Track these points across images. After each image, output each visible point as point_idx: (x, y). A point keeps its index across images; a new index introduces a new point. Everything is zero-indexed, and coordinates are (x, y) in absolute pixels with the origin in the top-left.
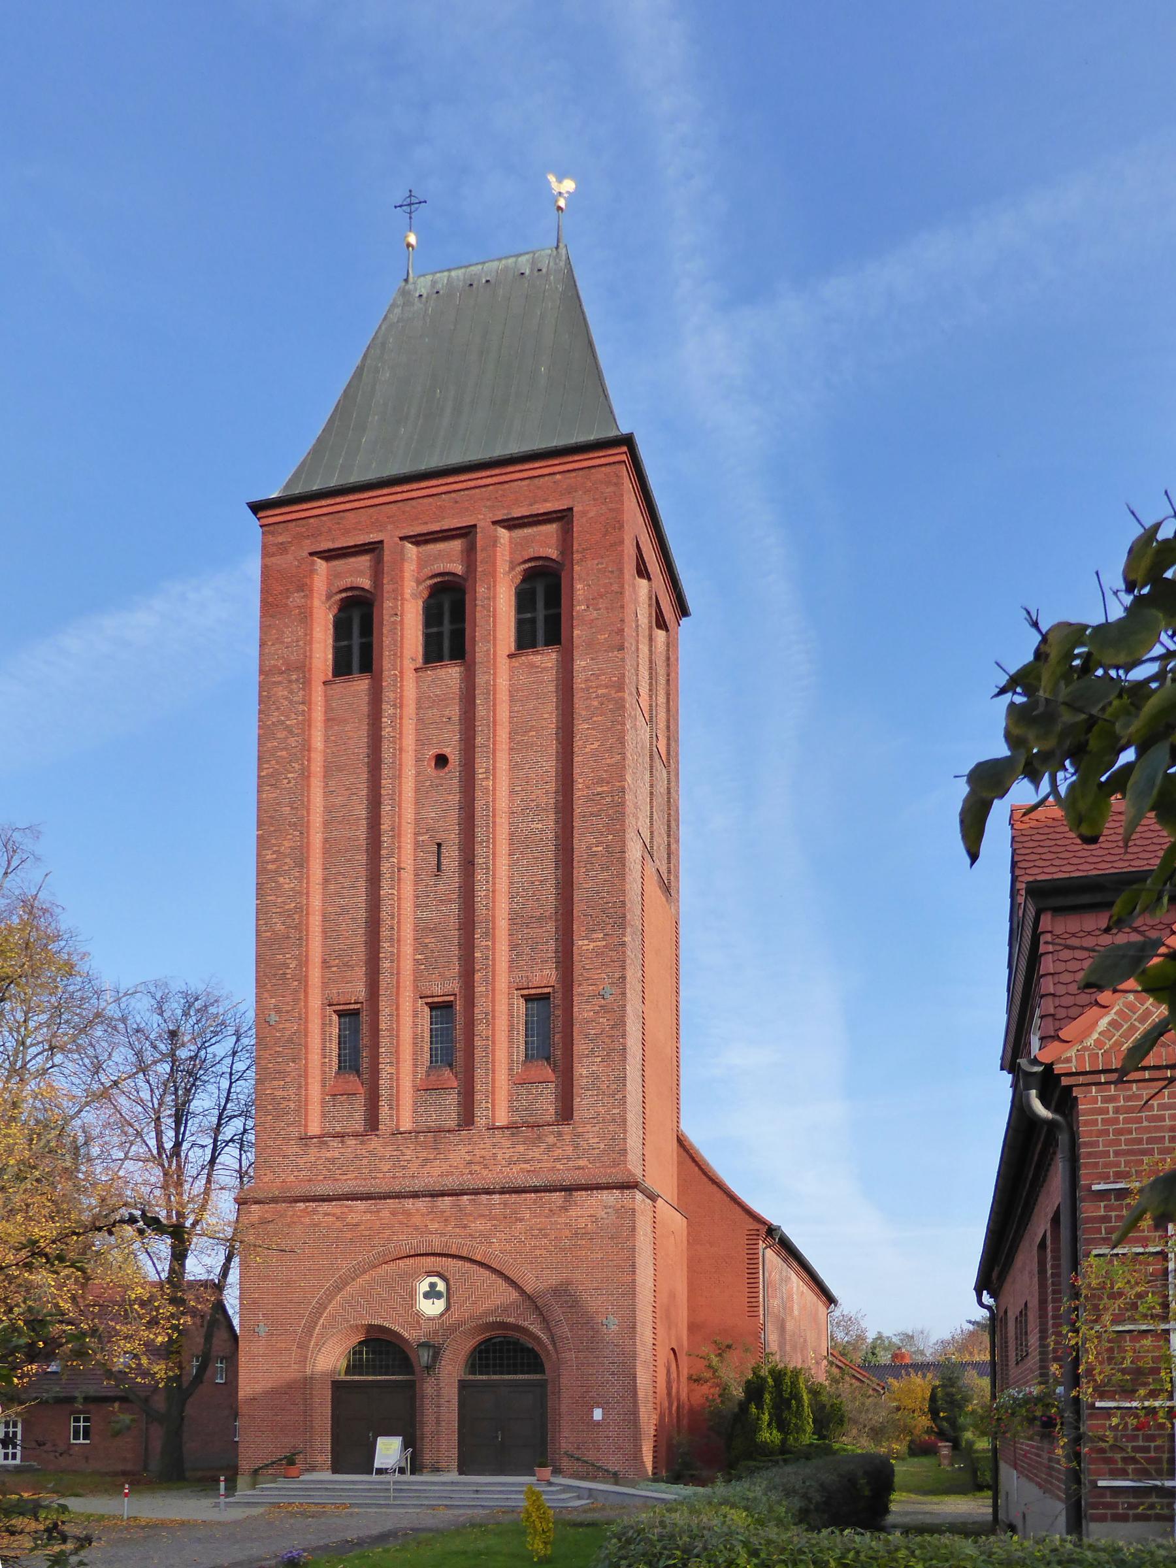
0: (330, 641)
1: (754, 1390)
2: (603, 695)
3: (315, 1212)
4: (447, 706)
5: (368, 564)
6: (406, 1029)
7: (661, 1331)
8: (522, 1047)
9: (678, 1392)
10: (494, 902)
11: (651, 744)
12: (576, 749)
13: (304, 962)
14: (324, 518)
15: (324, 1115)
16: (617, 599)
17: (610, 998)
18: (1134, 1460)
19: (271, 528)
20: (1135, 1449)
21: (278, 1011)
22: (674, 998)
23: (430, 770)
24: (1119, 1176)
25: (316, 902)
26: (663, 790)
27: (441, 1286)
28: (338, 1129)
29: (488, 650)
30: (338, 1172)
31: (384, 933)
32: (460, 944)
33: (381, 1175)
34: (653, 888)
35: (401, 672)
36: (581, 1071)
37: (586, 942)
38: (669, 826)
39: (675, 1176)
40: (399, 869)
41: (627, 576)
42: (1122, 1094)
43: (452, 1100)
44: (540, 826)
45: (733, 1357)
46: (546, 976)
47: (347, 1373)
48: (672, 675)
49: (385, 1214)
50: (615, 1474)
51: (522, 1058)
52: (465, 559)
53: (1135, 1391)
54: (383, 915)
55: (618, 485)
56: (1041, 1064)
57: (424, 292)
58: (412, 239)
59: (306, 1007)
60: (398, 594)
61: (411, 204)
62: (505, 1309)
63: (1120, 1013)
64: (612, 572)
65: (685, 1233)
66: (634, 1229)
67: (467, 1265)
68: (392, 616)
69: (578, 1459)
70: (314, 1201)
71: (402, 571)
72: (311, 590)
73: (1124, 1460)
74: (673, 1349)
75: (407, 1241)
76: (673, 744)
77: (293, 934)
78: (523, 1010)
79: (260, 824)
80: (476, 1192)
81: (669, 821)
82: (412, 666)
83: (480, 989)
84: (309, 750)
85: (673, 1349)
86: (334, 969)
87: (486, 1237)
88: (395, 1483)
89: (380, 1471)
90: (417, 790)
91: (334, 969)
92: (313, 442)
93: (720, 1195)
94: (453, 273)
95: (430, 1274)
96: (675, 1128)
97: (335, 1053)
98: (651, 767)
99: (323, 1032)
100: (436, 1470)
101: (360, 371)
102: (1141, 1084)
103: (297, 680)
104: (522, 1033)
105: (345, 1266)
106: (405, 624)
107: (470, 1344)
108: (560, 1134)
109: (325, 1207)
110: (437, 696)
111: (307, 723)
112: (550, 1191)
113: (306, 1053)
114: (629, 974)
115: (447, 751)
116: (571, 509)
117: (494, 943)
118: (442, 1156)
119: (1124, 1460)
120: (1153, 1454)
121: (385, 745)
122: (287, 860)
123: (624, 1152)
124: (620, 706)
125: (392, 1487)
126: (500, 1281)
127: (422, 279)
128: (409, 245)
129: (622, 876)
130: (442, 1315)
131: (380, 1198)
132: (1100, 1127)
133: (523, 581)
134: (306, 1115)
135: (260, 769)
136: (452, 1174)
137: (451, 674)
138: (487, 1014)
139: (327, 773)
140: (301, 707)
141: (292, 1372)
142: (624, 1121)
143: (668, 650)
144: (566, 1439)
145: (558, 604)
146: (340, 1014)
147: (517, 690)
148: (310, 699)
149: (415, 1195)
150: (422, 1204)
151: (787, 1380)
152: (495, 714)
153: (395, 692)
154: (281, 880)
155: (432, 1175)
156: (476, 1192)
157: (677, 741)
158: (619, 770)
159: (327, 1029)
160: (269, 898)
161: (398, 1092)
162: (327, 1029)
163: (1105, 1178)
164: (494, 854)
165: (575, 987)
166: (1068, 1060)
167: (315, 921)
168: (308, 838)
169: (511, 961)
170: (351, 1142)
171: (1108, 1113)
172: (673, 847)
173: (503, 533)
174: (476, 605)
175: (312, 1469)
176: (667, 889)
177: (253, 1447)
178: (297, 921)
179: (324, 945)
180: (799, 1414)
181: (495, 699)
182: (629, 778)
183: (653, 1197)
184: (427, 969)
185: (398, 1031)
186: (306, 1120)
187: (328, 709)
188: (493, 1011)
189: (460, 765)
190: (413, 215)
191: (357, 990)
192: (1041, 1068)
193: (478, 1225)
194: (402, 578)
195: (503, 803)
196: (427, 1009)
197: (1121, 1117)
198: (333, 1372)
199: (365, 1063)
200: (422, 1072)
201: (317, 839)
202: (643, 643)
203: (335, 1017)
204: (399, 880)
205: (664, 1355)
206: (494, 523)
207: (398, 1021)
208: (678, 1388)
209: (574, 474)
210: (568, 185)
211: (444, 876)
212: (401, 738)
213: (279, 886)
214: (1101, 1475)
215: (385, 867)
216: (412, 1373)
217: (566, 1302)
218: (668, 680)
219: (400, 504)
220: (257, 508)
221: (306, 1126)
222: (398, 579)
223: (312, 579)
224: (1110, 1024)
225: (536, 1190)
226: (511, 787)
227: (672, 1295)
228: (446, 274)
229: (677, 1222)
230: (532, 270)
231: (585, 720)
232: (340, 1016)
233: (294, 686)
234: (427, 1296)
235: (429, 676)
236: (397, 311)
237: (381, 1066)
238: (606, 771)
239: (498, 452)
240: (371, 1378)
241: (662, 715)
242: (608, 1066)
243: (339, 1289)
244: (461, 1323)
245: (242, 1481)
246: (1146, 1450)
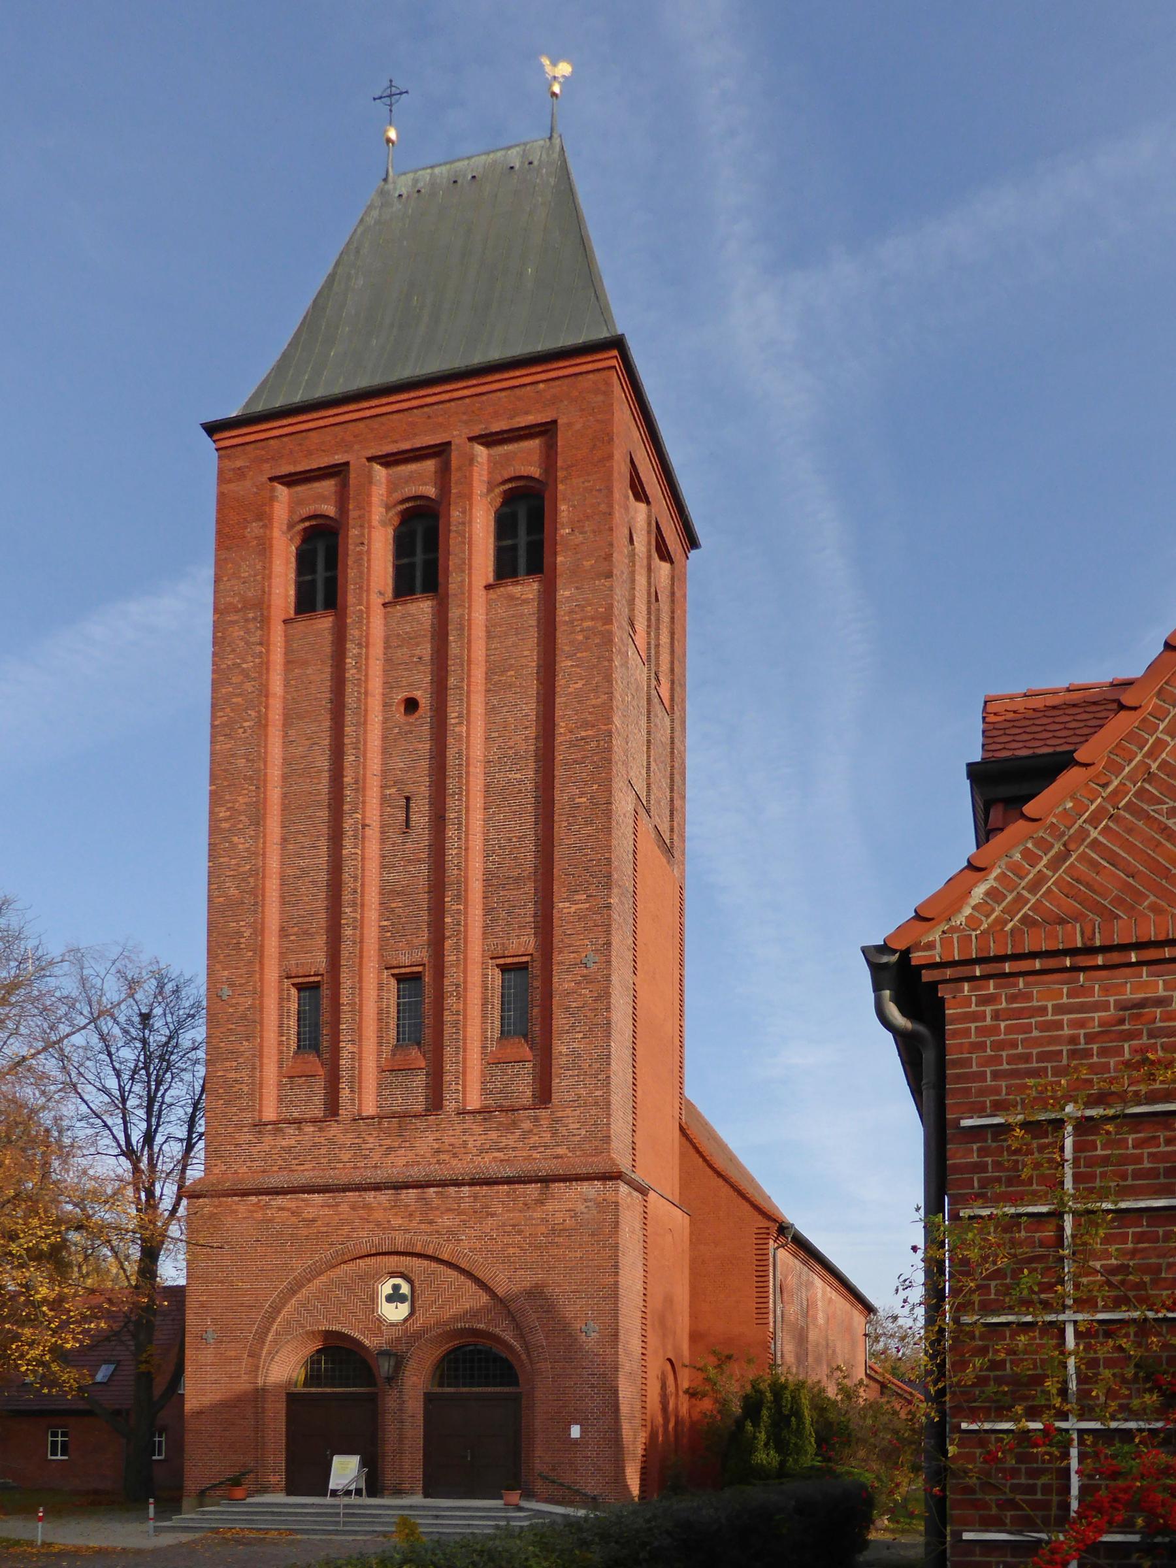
0: (292, 575)
1: (752, 1406)
2: (589, 629)
3: (267, 1206)
4: (418, 644)
5: (333, 489)
6: (370, 1000)
7: (653, 1340)
8: (497, 1023)
9: (676, 1408)
10: (466, 861)
11: (649, 686)
12: (558, 689)
13: (259, 930)
14: (285, 439)
15: (280, 1100)
16: (602, 519)
17: (593, 967)
18: (1013, 1504)
19: (229, 451)
20: (1015, 1488)
21: (232, 985)
22: (677, 972)
23: (399, 714)
24: (999, 1107)
25: (274, 863)
26: (666, 740)
27: (405, 1289)
28: (296, 1115)
29: (463, 581)
30: (294, 1162)
31: (347, 897)
32: (429, 909)
33: (341, 1165)
34: (649, 847)
35: (368, 608)
36: (560, 1048)
37: (567, 904)
38: (672, 780)
40: (364, 826)
41: (617, 495)
42: (1003, 993)
43: (419, 1081)
44: (518, 776)
45: (736, 1368)
46: (523, 943)
47: (305, 1385)
48: (678, 613)
49: (344, 1208)
50: (594, 1498)
51: (497, 1035)
52: (440, 484)
53: (1009, 1409)
54: (345, 876)
55: (608, 394)
56: (894, 951)
57: (404, 191)
58: (392, 134)
59: (261, 980)
60: (364, 522)
62: (474, 1314)
63: (1002, 878)
64: (600, 490)
65: (687, 1231)
66: (616, 1225)
67: (434, 1265)
68: (357, 545)
69: (554, 1482)
70: (267, 1194)
71: (369, 495)
72: (271, 519)
73: (1001, 1505)
74: (669, 1360)
75: (366, 1238)
76: (678, 689)
77: (249, 899)
78: (498, 982)
79: (213, 778)
80: (443, 1184)
81: (672, 774)
82: (381, 601)
83: (450, 958)
84: (267, 696)
85: (669, 1360)
86: (292, 938)
88: (346, 1506)
89: (334, 1493)
90: (384, 738)
91: (292, 938)
92: (278, 357)
93: (726, 1189)
94: (437, 170)
95: (393, 1275)
96: (677, 1116)
97: (293, 1031)
98: (649, 712)
99: (281, 1008)
100: (398, 1492)
101: (332, 278)
102: (1031, 979)
103: (254, 619)
104: (498, 1006)
105: (299, 1266)
106: (375, 554)
107: (439, 1352)
108: (536, 1119)
109: (280, 1201)
110: (407, 633)
111: (264, 666)
112: (524, 1182)
113: (262, 1031)
114: (616, 940)
115: (417, 694)
116: (555, 422)
117: (466, 908)
118: (407, 1144)
119: (1001, 1505)
120: (1039, 1496)
121: (349, 688)
122: (243, 818)
123: (607, 1139)
124: (608, 640)
125: (342, 1511)
126: (469, 1283)
127: (403, 177)
128: (389, 140)
129: (608, 830)
130: (406, 1320)
131: (338, 1191)
132: (973, 1039)
133: (503, 504)
134: (261, 1100)
135: (214, 717)
136: (418, 1163)
137: (422, 609)
138: (458, 986)
139: (288, 720)
140: (258, 648)
141: (243, 1384)
142: (608, 1104)
143: (673, 584)
144: (541, 1458)
145: (541, 529)
146: (300, 987)
147: (494, 626)
148: (268, 640)
149: (377, 1187)
150: (384, 1197)
151: (787, 1395)
152: (469, 651)
153: (360, 629)
154: (235, 839)
155: (397, 1165)
156: (443, 1184)
157: (683, 686)
158: (606, 713)
159: (285, 1004)
160: (222, 860)
161: (360, 1073)
162: (285, 1004)
163: (980, 1111)
164: (467, 808)
165: (555, 954)
166: (930, 946)
167: (273, 886)
168: (265, 793)
169: (485, 927)
170: (309, 1128)
171: (984, 1019)
172: (677, 803)
173: (480, 451)
174: (449, 531)
175: (264, 1490)
176: (669, 849)
177: (202, 1465)
178: (252, 884)
179: (282, 912)
180: (799, 1432)
181: (469, 635)
182: (617, 721)
183: (643, 1191)
185: (361, 1006)
186: (261, 1105)
187: (288, 651)
188: (465, 982)
189: (431, 711)
191: (318, 961)
192: (894, 958)
193: (446, 1221)
194: (370, 504)
195: (478, 750)
196: (393, 982)
197: (1003, 1025)
198: (289, 1383)
199: (325, 1042)
200: (387, 1050)
201: (275, 794)
202: (636, 575)
203: (294, 991)
204: (363, 837)
205: (656, 1366)
206: (471, 439)
207: (360, 995)
208: (677, 1404)
209: (558, 383)
210: (564, 69)
211: (413, 835)
212: (366, 681)
213: (234, 846)
214: (970, 1525)
215: (348, 824)
216: (375, 1385)
217: (542, 1306)
218: (673, 618)
219: (368, 421)
220: (212, 429)
221: (260, 1111)
222: (365, 506)
223: (272, 506)
224: (988, 894)
225: (509, 1181)
226: (486, 733)
227: (669, 1300)
228: (429, 171)
229: (679, 1219)
230: (522, 163)
231: (569, 657)
232: (299, 990)
233: (251, 626)
234: (390, 1299)
235: (399, 611)
236: (375, 213)
237: (342, 1044)
238: (590, 713)
239: (477, 358)
240: (328, 1390)
241: (665, 658)
242: (590, 1043)
243: (293, 1291)
244: (425, 1330)
245: (186, 1503)
246: (1031, 1489)
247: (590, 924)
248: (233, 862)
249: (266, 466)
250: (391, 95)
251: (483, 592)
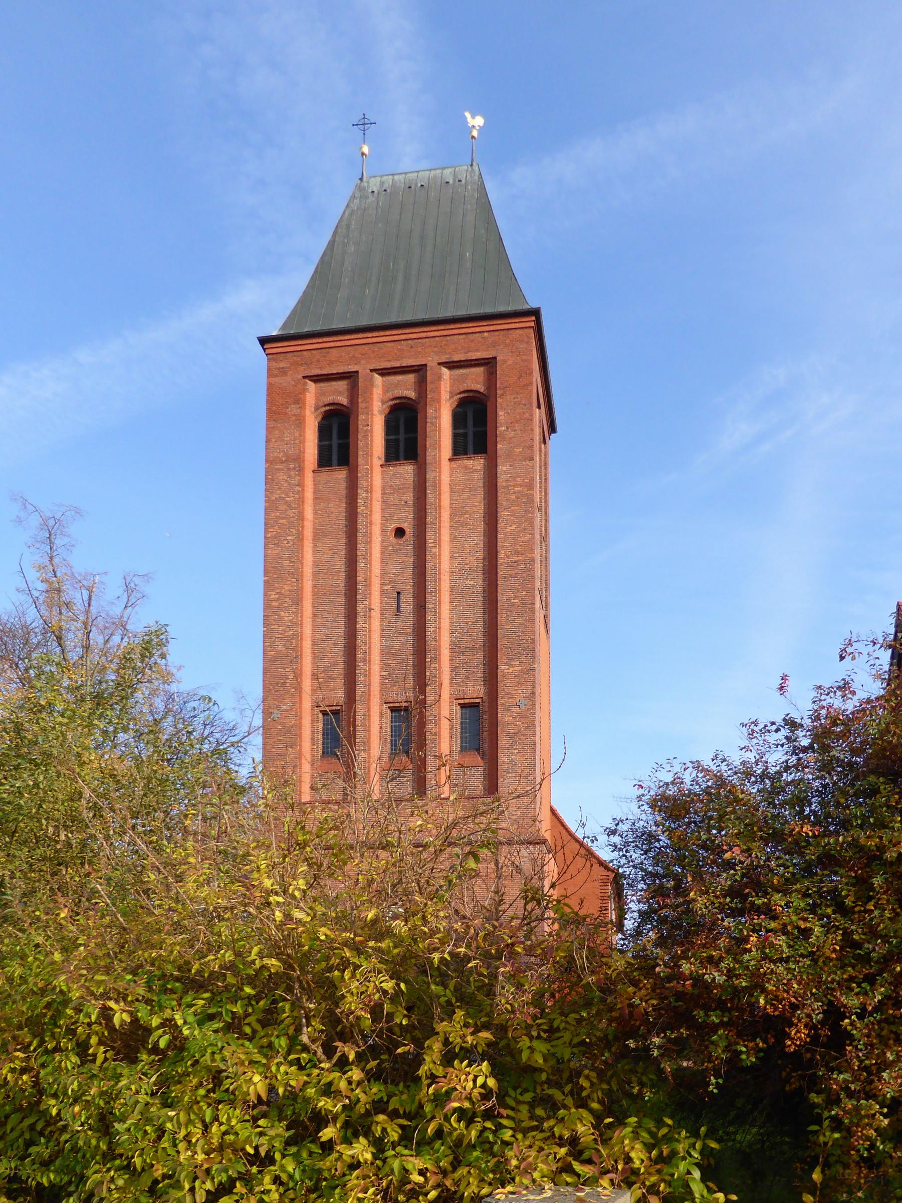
58: (366, 149)
61: (364, 124)
90: (382, 553)
189: (416, 535)
248: (281, 628)
250: (364, 124)
251: (448, 463)
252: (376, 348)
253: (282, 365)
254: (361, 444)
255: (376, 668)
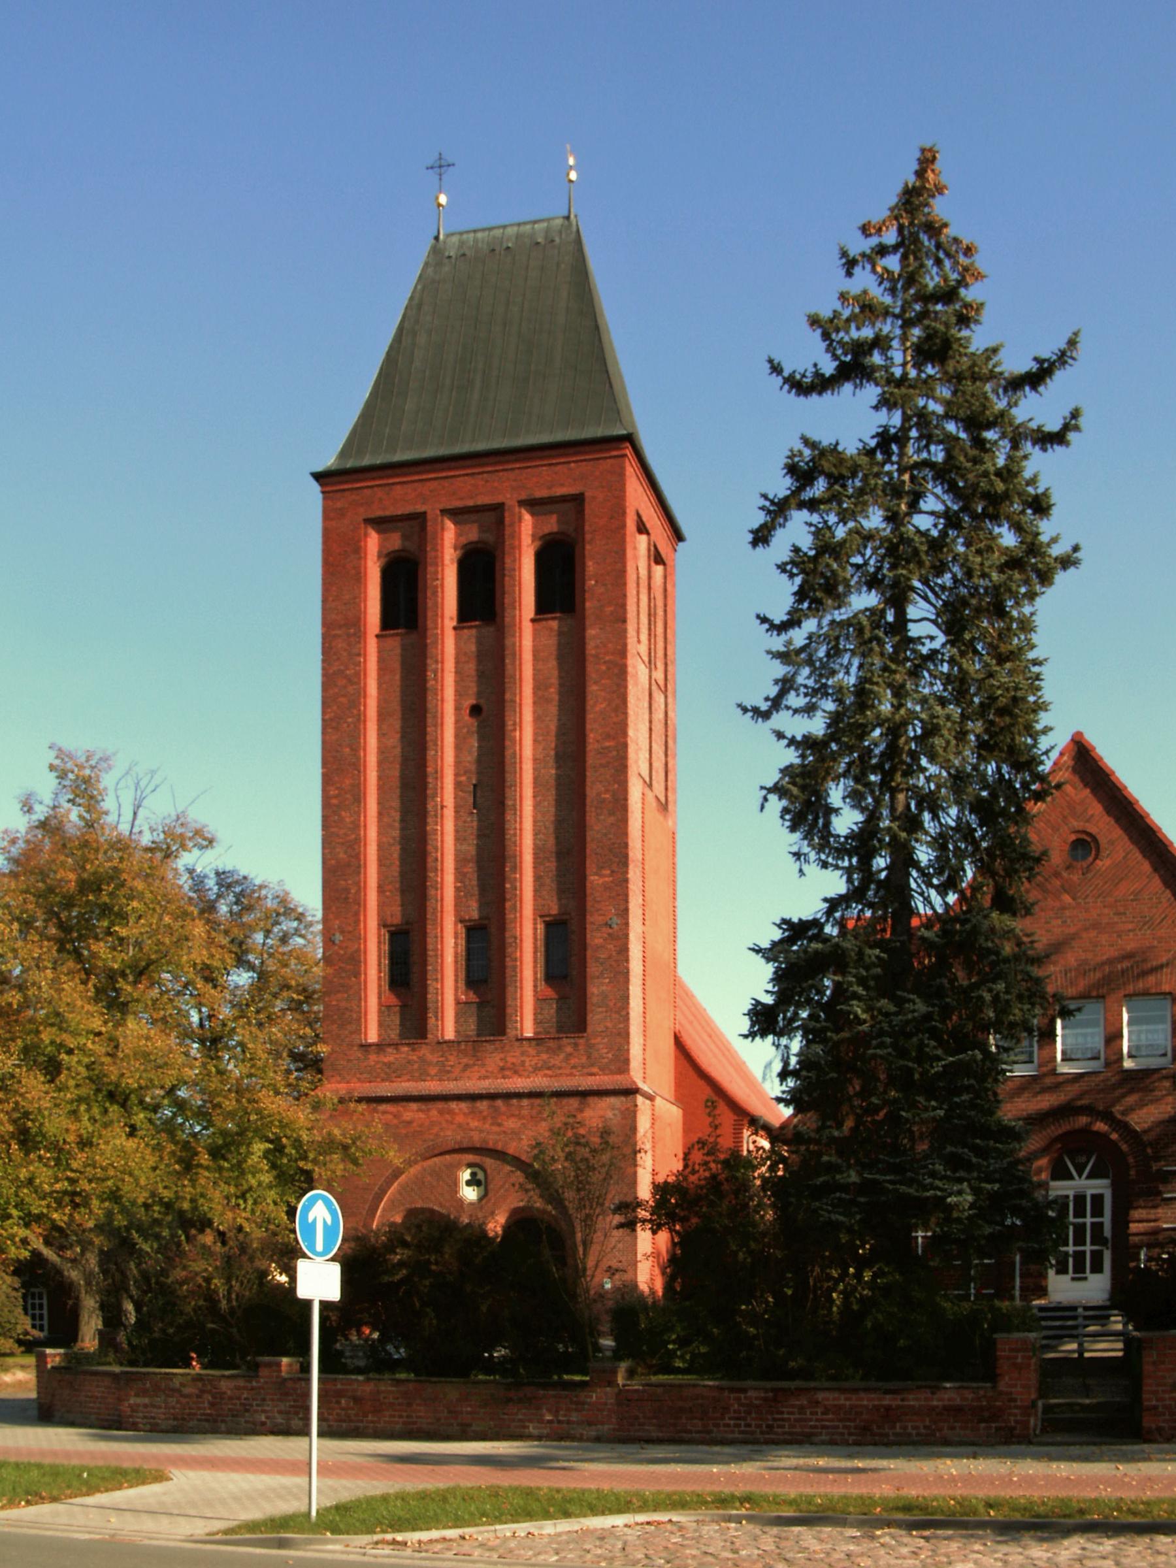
21: (342, 932)
26: (661, 716)
39: (673, 1071)
49: (434, 1113)
58: (443, 199)
61: (441, 166)
75: (451, 1136)
81: (666, 742)
87: (516, 1134)
90: (456, 736)
94: (479, 235)
108: (576, 1045)
122: (348, 796)
143: (665, 583)
150: (463, 1105)
176: (664, 807)
183: (651, 1098)
184: (465, 896)
189: (489, 715)
190: (444, 177)
204: (442, 816)
220: (318, 477)
228: (472, 235)
231: (596, 683)
234: (468, 1183)
247: (614, 894)
248: (342, 832)
249: (362, 510)
250: (441, 166)
251: (530, 624)
252: (446, 483)
253: (339, 505)
254: (430, 603)
255: (449, 878)
